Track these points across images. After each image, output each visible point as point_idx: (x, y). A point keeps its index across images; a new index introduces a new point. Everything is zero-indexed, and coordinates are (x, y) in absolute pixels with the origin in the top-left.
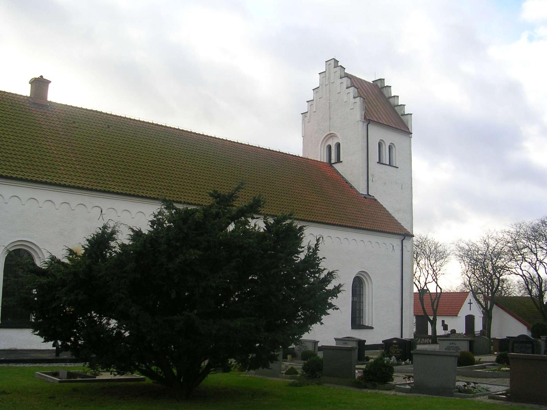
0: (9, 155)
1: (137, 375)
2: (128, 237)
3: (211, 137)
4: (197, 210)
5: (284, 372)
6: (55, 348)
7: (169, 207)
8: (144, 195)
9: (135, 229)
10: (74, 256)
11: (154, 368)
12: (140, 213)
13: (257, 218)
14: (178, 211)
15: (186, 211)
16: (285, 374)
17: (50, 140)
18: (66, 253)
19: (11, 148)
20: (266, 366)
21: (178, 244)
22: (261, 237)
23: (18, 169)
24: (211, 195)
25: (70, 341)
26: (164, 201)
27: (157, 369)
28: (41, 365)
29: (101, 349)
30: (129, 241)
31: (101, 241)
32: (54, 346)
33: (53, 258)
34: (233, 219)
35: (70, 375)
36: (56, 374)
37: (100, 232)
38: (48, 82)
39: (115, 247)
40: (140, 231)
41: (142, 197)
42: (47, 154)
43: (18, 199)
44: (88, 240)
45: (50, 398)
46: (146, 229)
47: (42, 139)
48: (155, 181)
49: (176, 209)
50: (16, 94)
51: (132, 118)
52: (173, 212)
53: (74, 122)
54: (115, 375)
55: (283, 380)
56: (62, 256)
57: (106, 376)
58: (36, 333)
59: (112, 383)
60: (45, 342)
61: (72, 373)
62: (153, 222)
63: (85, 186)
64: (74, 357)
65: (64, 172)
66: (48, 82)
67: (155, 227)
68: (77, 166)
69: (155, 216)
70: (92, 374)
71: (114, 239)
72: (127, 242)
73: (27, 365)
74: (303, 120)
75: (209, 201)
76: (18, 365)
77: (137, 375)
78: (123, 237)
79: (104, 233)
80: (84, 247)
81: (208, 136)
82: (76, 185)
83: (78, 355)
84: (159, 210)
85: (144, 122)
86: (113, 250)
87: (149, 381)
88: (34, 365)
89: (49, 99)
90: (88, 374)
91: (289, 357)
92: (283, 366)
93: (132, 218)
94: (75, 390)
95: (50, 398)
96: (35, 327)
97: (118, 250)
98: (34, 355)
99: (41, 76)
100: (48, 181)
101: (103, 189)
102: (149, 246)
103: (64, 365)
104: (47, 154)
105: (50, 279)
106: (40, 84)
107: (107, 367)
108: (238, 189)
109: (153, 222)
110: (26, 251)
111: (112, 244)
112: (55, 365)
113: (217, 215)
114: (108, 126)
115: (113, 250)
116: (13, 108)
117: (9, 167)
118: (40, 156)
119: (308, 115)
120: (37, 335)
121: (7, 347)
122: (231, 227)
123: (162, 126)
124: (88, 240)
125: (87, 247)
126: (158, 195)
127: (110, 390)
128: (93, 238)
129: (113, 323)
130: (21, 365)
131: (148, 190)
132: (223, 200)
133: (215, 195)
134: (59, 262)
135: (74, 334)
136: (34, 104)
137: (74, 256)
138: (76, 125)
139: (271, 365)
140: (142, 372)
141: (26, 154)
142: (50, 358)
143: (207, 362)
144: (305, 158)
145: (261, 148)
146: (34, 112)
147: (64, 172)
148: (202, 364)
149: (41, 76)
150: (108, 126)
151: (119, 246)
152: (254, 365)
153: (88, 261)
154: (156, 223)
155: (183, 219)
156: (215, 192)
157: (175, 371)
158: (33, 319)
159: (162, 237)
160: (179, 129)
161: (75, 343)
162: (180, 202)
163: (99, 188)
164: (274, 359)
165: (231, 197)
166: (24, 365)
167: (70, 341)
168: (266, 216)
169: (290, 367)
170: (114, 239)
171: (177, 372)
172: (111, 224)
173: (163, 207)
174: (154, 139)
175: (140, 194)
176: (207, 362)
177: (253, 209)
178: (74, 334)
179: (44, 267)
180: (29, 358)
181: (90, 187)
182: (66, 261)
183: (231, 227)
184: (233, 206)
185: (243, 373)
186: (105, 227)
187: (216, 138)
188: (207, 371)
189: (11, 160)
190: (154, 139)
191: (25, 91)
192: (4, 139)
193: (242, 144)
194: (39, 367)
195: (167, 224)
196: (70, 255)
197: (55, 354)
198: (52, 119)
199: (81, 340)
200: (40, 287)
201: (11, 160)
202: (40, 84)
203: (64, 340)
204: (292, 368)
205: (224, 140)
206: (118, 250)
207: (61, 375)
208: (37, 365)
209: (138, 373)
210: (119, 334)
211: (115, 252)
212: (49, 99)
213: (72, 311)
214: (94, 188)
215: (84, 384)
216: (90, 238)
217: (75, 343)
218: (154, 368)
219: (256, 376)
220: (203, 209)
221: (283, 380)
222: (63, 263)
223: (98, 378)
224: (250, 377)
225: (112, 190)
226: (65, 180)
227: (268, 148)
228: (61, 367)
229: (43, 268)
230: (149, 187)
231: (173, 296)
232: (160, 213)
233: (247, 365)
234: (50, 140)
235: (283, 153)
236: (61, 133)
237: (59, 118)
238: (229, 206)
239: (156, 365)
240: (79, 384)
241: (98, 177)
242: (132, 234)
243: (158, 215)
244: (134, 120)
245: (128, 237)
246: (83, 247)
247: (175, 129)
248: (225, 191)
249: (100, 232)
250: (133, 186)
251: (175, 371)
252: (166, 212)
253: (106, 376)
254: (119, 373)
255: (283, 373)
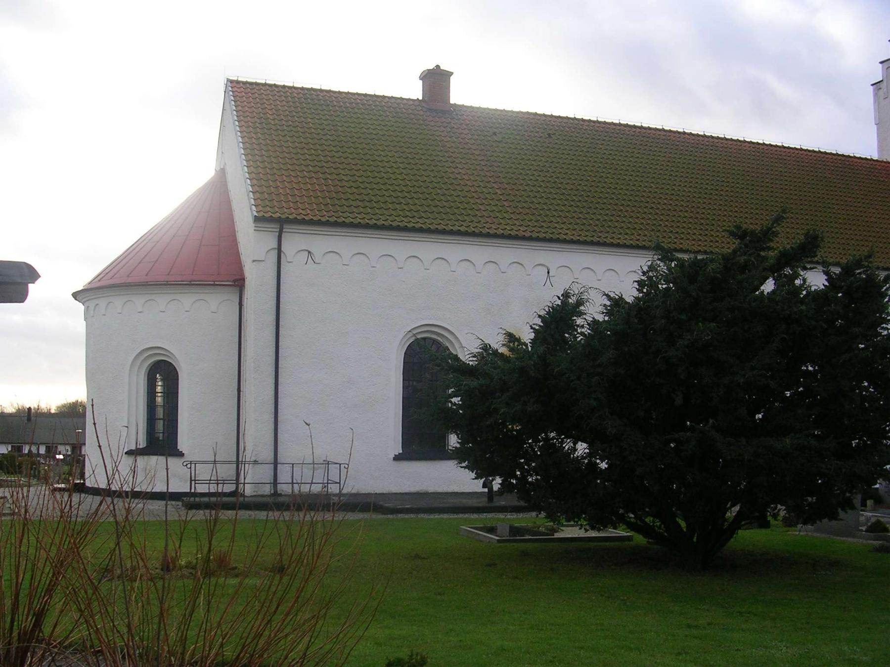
0: (399, 194)
1: (621, 532)
2: (601, 309)
3: (718, 138)
4: (712, 260)
5: (864, 528)
6: (486, 490)
7: (666, 255)
8: (615, 241)
9: (612, 295)
10: (516, 344)
11: (649, 520)
12: (515, 265)
13: (811, 269)
14: (681, 264)
15: (695, 263)
16: (866, 531)
17: (459, 166)
18: (501, 338)
19: (401, 182)
20: (833, 516)
21: (684, 317)
22: (818, 297)
23: (415, 214)
24: (732, 234)
25: (515, 477)
26: (658, 248)
27: (654, 522)
28: (467, 516)
29: (564, 489)
30: (602, 316)
31: (560, 318)
32: (484, 486)
33: (486, 347)
34: (774, 270)
35: (515, 531)
36: (492, 530)
37: (559, 302)
38: (449, 74)
39: (583, 327)
40: (621, 298)
41: (612, 245)
42: (457, 187)
43: (418, 261)
44: (540, 316)
45: (489, 565)
46: (630, 294)
47: (447, 164)
48: (631, 217)
49: (678, 259)
50: (401, 99)
51: (585, 118)
52: (673, 265)
53: (495, 134)
54: (586, 530)
55: (863, 542)
56: (497, 342)
57: (571, 532)
58: (464, 465)
59: (592, 544)
60: (476, 478)
61: (516, 528)
62: (641, 283)
63: (520, 234)
64: (522, 503)
65: (485, 214)
66: (449, 74)
67: (645, 290)
68: (505, 203)
69: (644, 273)
70: (547, 529)
71: (580, 314)
72: (600, 318)
73: (445, 516)
74: (876, 95)
75: (729, 246)
76: (432, 517)
77: (621, 532)
78: (595, 310)
79: (565, 303)
80: (534, 329)
81: (712, 137)
82: (507, 233)
83: (530, 500)
84: (649, 263)
85: (605, 123)
86: (579, 331)
87: (640, 539)
88: (456, 516)
89: (452, 101)
90: (542, 529)
91: (869, 503)
92: (862, 519)
93: (608, 278)
94: (525, 554)
95: (489, 565)
96: (459, 455)
97: (587, 331)
98: (464, 501)
99: (438, 66)
100: (462, 229)
101: (548, 236)
102: (636, 321)
103: (503, 517)
104: (457, 187)
105: (482, 381)
106: (436, 80)
107: (573, 517)
108: (778, 220)
109: (641, 283)
110: (434, 341)
111: (579, 321)
112: (490, 516)
113: (744, 268)
114: (549, 135)
115: (579, 331)
116: (399, 120)
117: (401, 213)
118: (446, 192)
119: (884, 85)
120: (465, 467)
121: (413, 489)
122: (769, 286)
123: (635, 127)
124: (540, 316)
125: (537, 328)
126: (638, 240)
127: (579, 555)
128: (549, 313)
129: (582, 448)
130: (437, 516)
131: (621, 234)
132: (753, 240)
133: (740, 234)
134: (495, 352)
135: (520, 467)
136: (430, 110)
137: (516, 344)
138: (498, 137)
139: (842, 514)
140: (631, 526)
141: (425, 190)
142: (480, 505)
143: (737, 508)
144: (882, 162)
145: (805, 150)
146: (432, 124)
147: (485, 214)
148: (728, 514)
149: (438, 66)
150: (549, 135)
151: (588, 324)
152: (809, 517)
153: (542, 349)
154: (646, 284)
155: (689, 274)
156: (738, 227)
157: (683, 524)
158: (453, 441)
159: (657, 307)
160: (663, 130)
161: (522, 480)
162: (682, 251)
163: (541, 235)
164: (848, 505)
165: (767, 234)
166: (442, 516)
167: (515, 477)
168: (825, 264)
169: (873, 520)
170: (580, 314)
171: (687, 527)
172: (576, 290)
173: (656, 257)
174: (625, 150)
175: (609, 241)
176: (737, 508)
177: (806, 252)
178: (520, 467)
179: (472, 362)
180: (447, 505)
181: (528, 234)
182: (503, 350)
183: (769, 286)
184: (769, 248)
185: (793, 528)
186: (566, 295)
187: (727, 139)
188: (737, 524)
189: (402, 201)
190: (625, 150)
191: (414, 91)
192: (389, 170)
193: (771, 145)
194: (466, 519)
195: (663, 286)
196: (510, 342)
197: (486, 499)
198: (460, 131)
199: (531, 476)
200: (467, 395)
201: (402, 201)
202: (436, 80)
203: (507, 475)
204: (878, 522)
205: (679, 133)
206: (587, 331)
207: (499, 532)
208: (461, 516)
209: (624, 527)
210: (593, 466)
211: (582, 334)
212: (452, 101)
213: (516, 430)
214: (534, 235)
215: (536, 545)
216: (542, 313)
217: (522, 480)
218: (649, 520)
219: (816, 534)
220: (724, 259)
221: (863, 542)
222: (502, 354)
223: (557, 535)
224: (804, 535)
225: (563, 237)
226: (487, 225)
227: (799, 147)
228: (499, 519)
229: (471, 363)
230: (622, 228)
231: (679, 400)
232: (651, 268)
233: (802, 515)
234: (459, 166)
235: (843, 155)
236: (477, 152)
237: (470, 130)
238: (763, 249)
239: (651, 516)
240: (530, 546)
241: (539, 218)
242: (608, 303)
243: (648, 272)
244: (590, 121)
245: (601, 309)
246: (532, 328)
247: (656, 129)
248: (753, 225)
249: (559, 302)
250: (596, 228)
251: (683, 524)
252: (662, 267)
253: (571, 532)
254: (593, 528)
255: (862, 530)
